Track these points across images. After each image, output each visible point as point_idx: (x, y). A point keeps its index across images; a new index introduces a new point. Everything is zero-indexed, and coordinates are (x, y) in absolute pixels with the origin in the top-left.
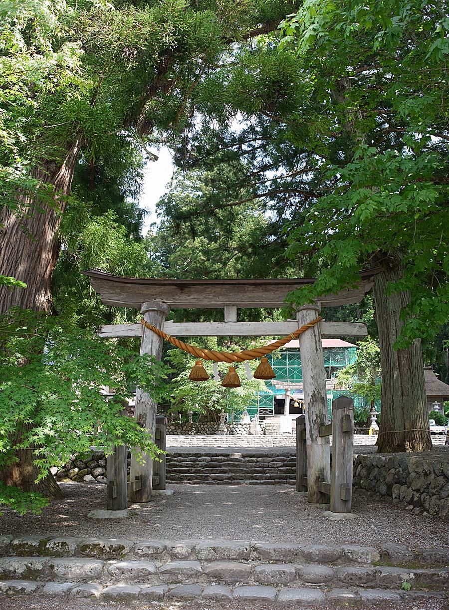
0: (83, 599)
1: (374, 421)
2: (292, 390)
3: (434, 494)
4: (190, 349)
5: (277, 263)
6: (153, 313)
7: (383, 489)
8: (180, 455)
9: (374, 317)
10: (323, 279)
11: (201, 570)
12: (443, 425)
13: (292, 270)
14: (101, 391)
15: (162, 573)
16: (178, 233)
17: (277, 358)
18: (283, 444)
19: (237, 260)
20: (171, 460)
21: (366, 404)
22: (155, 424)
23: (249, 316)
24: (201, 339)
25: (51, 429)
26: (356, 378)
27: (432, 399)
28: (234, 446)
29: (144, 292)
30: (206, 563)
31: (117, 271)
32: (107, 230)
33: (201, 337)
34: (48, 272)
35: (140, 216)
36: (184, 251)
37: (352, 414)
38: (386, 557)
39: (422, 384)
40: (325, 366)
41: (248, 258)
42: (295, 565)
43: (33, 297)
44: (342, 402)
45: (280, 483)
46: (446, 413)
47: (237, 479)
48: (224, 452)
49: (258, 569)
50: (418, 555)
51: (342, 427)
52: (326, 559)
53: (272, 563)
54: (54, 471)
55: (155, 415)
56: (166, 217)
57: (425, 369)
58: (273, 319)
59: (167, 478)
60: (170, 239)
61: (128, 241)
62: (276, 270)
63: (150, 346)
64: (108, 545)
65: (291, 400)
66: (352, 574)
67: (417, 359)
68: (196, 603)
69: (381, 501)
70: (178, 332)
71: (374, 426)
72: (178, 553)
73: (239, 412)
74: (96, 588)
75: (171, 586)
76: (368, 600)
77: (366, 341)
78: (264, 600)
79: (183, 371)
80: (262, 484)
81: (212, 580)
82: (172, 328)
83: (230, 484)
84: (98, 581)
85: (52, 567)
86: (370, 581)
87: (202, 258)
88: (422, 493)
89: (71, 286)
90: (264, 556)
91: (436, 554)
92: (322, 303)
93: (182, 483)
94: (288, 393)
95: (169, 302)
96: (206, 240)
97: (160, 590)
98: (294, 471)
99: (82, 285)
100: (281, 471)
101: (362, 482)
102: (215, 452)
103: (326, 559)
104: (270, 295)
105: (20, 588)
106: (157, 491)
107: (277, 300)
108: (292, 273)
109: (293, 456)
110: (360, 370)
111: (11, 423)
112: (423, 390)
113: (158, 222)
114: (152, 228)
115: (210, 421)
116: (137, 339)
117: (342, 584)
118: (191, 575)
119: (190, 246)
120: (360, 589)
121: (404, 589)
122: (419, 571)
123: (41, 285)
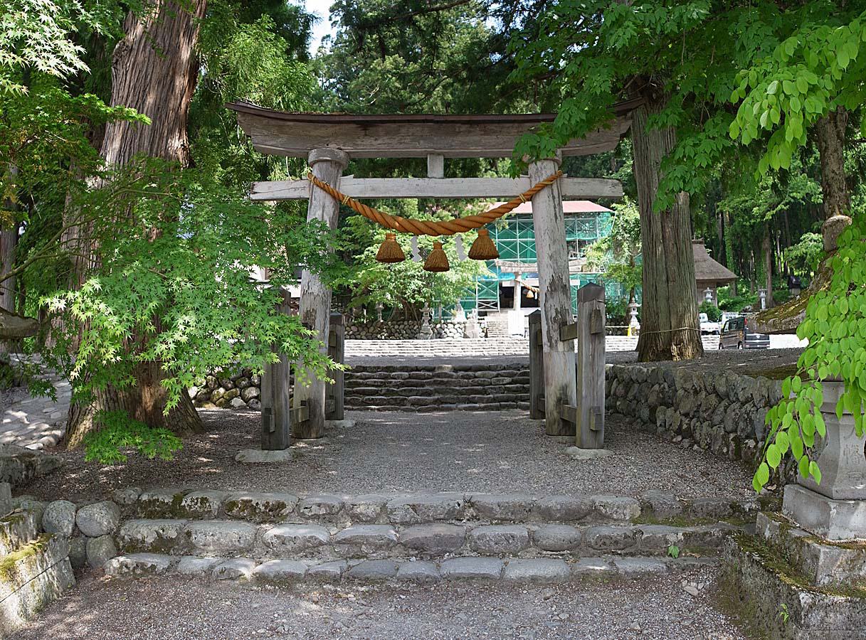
0: (228, 582)
1: (634, 317)
2: (523, 274)
3: (705, 420)
4: (378, 216)
5: (503, 92)
6: (325, 165)
7: (645, 413)
8: (365, 369)
9: (633, 171)
10: (568, 113)
11: (395, 539)
12: (715, 321)
13: (525, 103)
14: (252, 275)
15: (339, 542)
16: (359, 50)
17: (504, 228)
18: (512, 351)
19: (445, 87)
20: (351, 377)
21: (624, 292)
22: (328, 325)
23: (463, 168)
24: (394, 202)
25: (184, 334)
26: (610, 256)
27: (703, 284)
28: (442, 354)
29: (312, 133)
30: (402, 528)
31: (274, 104)
32: (260, 44)
33: (394, 199)
34: (183, 106)
35: (307, 26)
36: (370, 75)
37: (602, 307)
38: (648, 510)
39: (691, 263)
40: (568, 239)
41: (462, 85)
42: (528, 527)
43: (164, 142)
44: (591, 291)
45: (508, 407)
46: (720, 304)
47: (446, 403)
48: (427, 365)
49: (476, 533)
50: (688, 507)
51: (590, 328)
52: (572, 516)
53: (496, 524)
54: (193, 392)
55: (328, 311)
56: (345, 27)
57: (695, 243)
58: (497, 173)
59: (346, 402)
60: (349, 59)
61: (290, 61)
62: (502, 103)
63: (321, 210)
64: (262, 502)
65: (523, 288)
66: (605, 537)
67: (685, 228)
68: (388, 588)
69: (643, 431)
70: (361, 192)
71: (635, 324)
72: (361, 514)
73: (449, 306)
74: (246, 566)
75: (352, 563)
76: (626, 573)
77: (624, 203)
78: (485, 577)
79: (369, 246)
80: (483, 409)
81: (412, 553)
82: (352, 187)
83: (435, 409)
84: (250, 555)
85: (189, 534)
86: (629, 547)
87: (397, 84)
88: (692, 419)
89: (214, 127)
90: (482, 513)
91: (707, 504)
92: (562, 151)
93: (368, 409)
94: (519, 279)
95: (349, 149)
96: (401, 60)
97: (334, 569)
98: (527, 390)
99: (227, 124)
100: (509, 390)
101: (618, 403)
102: (414, 365)
103: (572, 516)
104: (491, 139)
105: (149, 565)
106: (332, 422)
107: (501, 146)
108: (523, 106)
109: (526, 368)
110: (616, 245)
111: (129, 324)
112: (692, 273)
113: (333, 33)
114: (324, 42)
115: (408, 318)
116: (304, 201)
117: (592, 551)
118: (381, 546)
119: (379, 68)
120: (617, 557)
121: (671, 555)
122: (690, 530)
123: (175, 123)
